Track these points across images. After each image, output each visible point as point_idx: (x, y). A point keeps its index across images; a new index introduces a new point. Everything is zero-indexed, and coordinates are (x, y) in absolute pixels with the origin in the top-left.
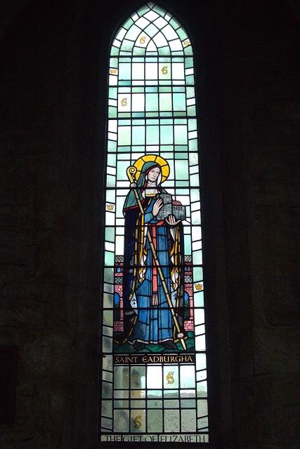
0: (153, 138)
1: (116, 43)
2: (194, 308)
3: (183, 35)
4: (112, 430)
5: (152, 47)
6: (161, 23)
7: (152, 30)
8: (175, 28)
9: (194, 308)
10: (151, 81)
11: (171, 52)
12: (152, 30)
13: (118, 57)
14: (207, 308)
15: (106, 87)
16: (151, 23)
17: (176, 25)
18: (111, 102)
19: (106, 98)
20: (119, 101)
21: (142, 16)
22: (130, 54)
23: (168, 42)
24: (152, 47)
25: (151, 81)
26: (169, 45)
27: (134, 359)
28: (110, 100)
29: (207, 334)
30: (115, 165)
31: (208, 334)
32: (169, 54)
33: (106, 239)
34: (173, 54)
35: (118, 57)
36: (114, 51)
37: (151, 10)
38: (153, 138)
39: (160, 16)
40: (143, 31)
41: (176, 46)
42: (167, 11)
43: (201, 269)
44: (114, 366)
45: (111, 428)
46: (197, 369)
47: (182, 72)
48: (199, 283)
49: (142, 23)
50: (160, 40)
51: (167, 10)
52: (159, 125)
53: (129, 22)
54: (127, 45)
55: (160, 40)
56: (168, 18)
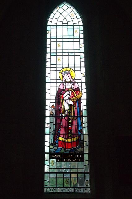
0: (65, 61)
1: (50, 19)
2: (82, 99)
3: (78, 15)
4: (49, 186)
5: (65, 21)
6: (69, 11)
7: (65, 14)
8: (75, 13)
9: (82, 99)
10: (65, 40)
11: (73, 24)
12: (65, 14)
13: (51, 25)
14: (89, 154)
15: (46, 39)
16: (65, 11)
17: (76, 12)
18: (47, 75)
19: (45, 44)
20: (51, 46)
21: (61, 8)
22: (56, 24)
23: (72, 19)
24: (65, 21)
25: (65, 40)
26: (72, 21)
27: (60, 156)
28: (47, 74)
29: (88, 127)
30: (49, 165)
31: (89, 127)
32: (73, 25)
33: (45, 164)
34: (74, 24)
35: (51, 25)
36: (49, 23)
37: (65, 5)
38: (65, 61)
39: (69, 8)
40: (61, 14)
41: (75, 21)
42: (72, 5)
43: (87, 155)
44: (49, 159)
45: (49, 165)
46: (82, 89)
47: (79, 32)
48: (83, 74)
49: (61, 11)
50: (69, 18)
51: (72, 4)
52: (68, 42)
53: (56, 10)
54: (54, 21)
55: (69, 18)
56: (72, 8)
